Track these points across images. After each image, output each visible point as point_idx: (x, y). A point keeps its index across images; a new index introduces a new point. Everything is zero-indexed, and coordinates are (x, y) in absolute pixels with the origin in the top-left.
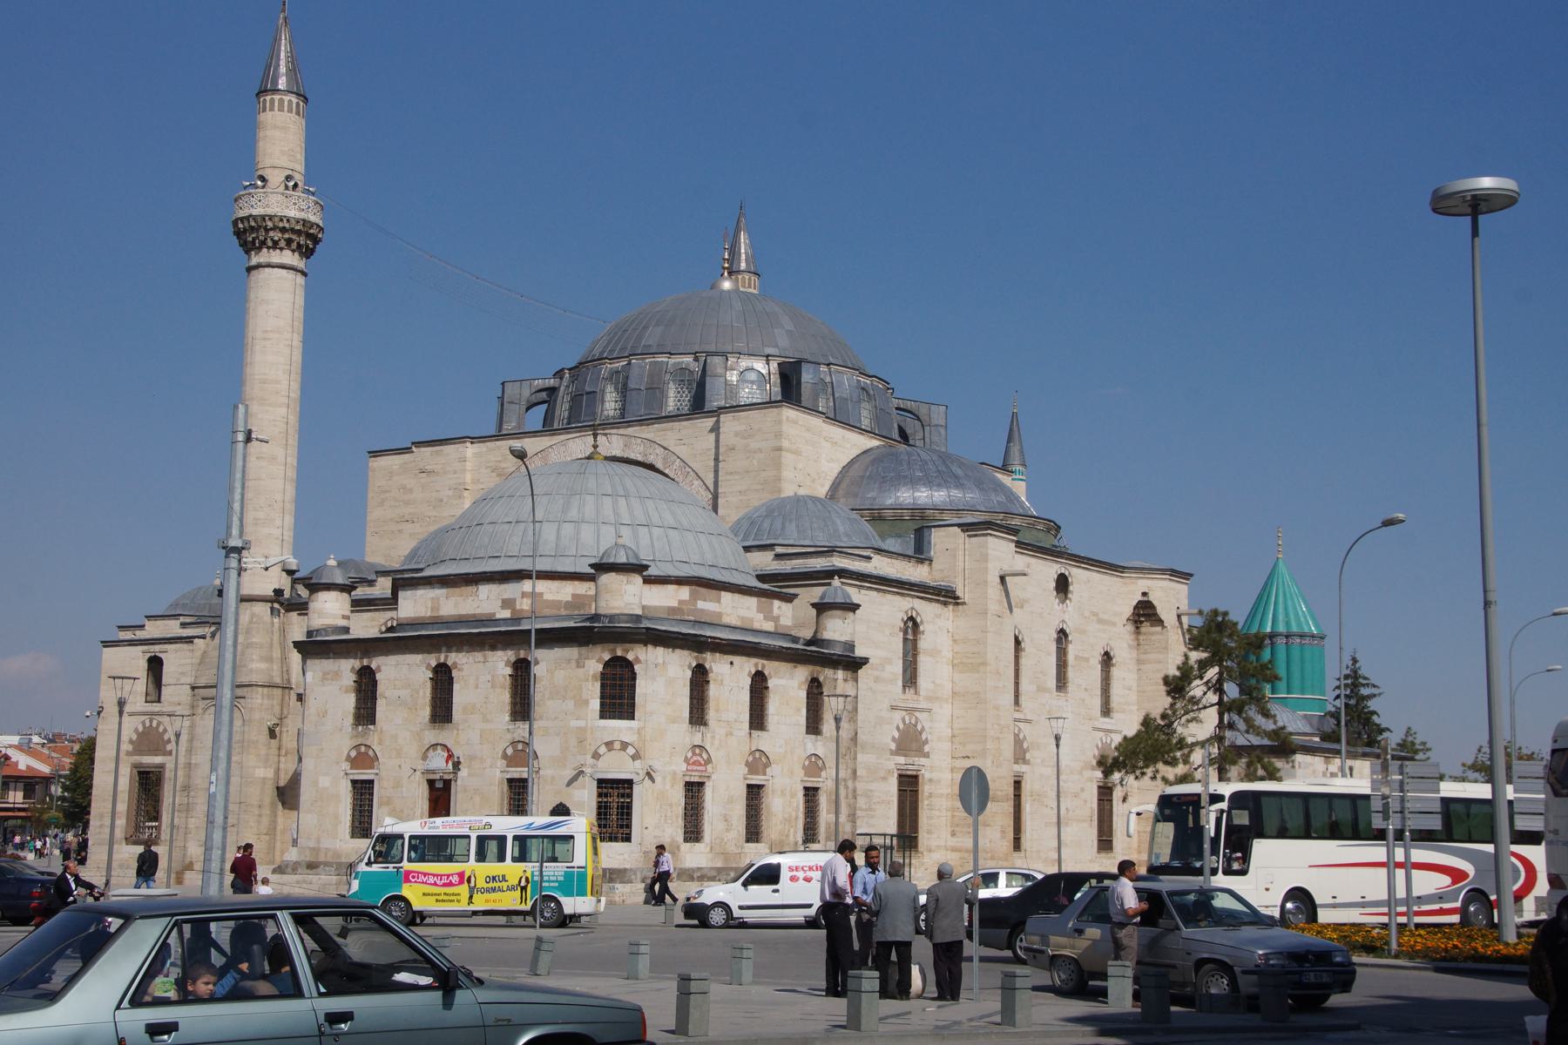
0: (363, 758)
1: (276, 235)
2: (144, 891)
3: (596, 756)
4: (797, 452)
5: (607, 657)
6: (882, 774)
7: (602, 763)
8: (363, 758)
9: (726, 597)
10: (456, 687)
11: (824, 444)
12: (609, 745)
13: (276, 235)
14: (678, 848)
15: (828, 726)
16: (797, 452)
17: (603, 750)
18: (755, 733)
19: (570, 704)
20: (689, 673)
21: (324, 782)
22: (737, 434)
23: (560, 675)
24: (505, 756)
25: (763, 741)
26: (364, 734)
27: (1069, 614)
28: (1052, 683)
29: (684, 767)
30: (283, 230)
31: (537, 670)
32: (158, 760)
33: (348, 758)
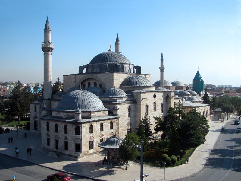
0: (48, 135)
1: (46, 50)
2: (88, 82)
3: (75, 140)
4: (116, 79)
5: (76, 126)
6: (124, 130)
7: (76, 141)
8: (48, 135)
9: (96, 113)
10: (58, 127)
11: (120, 77)
12: (77, 139)
13: (46, 50)
14: (88, 151)
15: (114, 127)
16: (116, 79)
17: (76, 139)
18: (101, 132)
19: (72, 132)
20: (89, 126)
21: (44, 137)
22: (108, 77)
23: (70, 128)
24: (64, 138)
25: (103, 133)
26: (48, 132)
27: (156, 100)
28: (153, 110)
29: (89, 140)
30: (47, 49)
31: (68, 127)
32: (37, 120)
33: (47, 135)
